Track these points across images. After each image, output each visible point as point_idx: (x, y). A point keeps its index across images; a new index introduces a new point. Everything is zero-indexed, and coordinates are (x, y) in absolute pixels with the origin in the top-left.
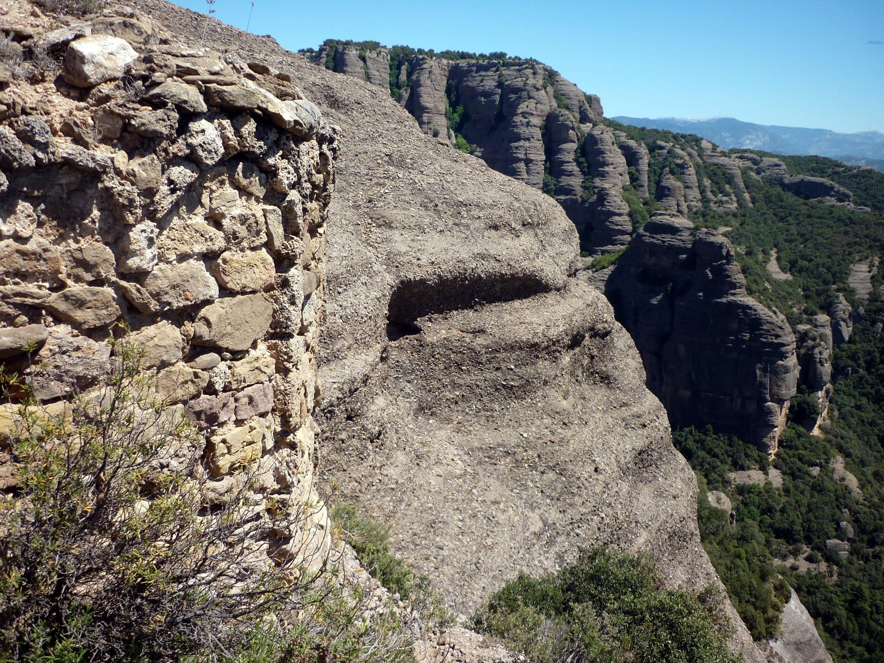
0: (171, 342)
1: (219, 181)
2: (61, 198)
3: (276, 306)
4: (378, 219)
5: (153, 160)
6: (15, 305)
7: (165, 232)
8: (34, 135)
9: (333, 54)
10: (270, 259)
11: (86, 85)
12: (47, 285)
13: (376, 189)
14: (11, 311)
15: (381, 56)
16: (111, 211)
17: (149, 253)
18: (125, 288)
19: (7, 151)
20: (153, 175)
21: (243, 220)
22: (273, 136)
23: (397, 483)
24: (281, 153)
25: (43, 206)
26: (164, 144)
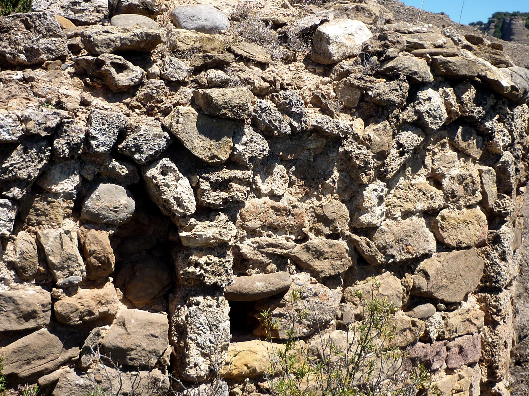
1: (441, 144)
2: (309, 161)
5: (386, 126)
6: (268, 255)
7: (392, 191)
8: (291, 107)
9: (500, 25)
10: (484, 217)
11: (329, 62)
12: (293, 237)
14: (264, 259)
16: (348, 172)
17: (378, 210)
18: (357, 242)
20: (386, 140)
21: (461, 179)
22: (491, 101)
24: (497, 117)
25: (294, 168)
26: (395, 112)
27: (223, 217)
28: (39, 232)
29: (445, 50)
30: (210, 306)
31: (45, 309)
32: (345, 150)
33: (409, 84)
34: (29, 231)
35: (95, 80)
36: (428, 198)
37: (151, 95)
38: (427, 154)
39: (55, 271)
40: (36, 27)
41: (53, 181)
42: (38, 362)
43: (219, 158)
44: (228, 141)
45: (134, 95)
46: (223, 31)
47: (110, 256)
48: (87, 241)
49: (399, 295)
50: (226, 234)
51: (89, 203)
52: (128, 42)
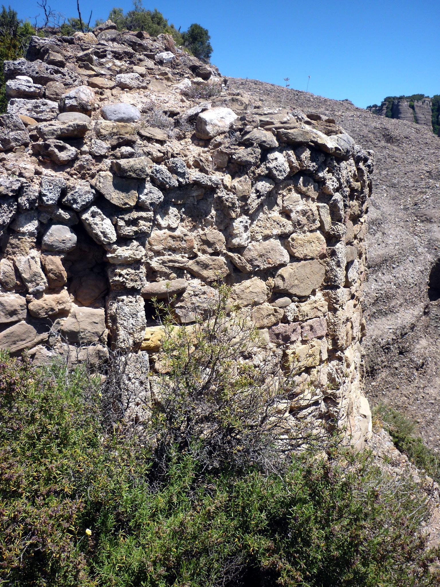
0: (260, 290)
1: (288, 190)
2: (194, 204)
3: (328, 268)
4: (422, 217)
5: (246, 178)
6: (169, 267)
7: (255, 222)
8: (177, 168)
9: (391, 106)
10: (322, 238)
11: (207, 138)
12: (187, 255)
13: (420, 196)
14: (168, 271)
15: (425, 104)
16: (222, 211)
17: (245, 235)
18: (231, 257)
19: (163, 179)
20: (246, 188)
21: (304, 213)
22: (321, 159)
23: (435, 399)
24: (327, 169)
25: (183, 210)
26: (252, 168)
27: (135, 243)
28: (15, 259)
29: (288, 125)
30: (131, 302)
31: (23, 308)
32: (218, 196)
33: (261, 149)
34: (8, 259)
35: (45, 157)
36: (281, 226)
37: (83, 166)
38: (279, 196)
39: (27, 283)
40: (6, 124)
41: (21, 225)
42: (21, 343)
43: (129, 205)
44: (134, 193)
45: (72, 166)
46: (136, 121)
47: (62, 272)
48: (47, 263)
49: (264, 292)
50: (138, 255)
51: (45, 238)
52: (65, 131)
